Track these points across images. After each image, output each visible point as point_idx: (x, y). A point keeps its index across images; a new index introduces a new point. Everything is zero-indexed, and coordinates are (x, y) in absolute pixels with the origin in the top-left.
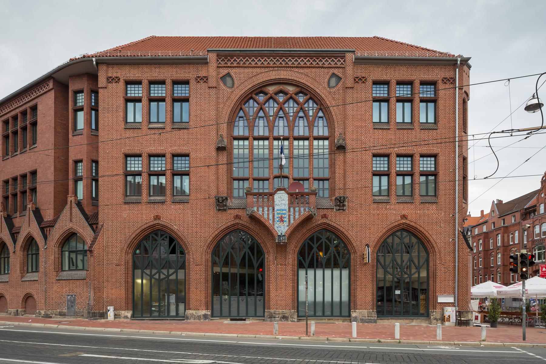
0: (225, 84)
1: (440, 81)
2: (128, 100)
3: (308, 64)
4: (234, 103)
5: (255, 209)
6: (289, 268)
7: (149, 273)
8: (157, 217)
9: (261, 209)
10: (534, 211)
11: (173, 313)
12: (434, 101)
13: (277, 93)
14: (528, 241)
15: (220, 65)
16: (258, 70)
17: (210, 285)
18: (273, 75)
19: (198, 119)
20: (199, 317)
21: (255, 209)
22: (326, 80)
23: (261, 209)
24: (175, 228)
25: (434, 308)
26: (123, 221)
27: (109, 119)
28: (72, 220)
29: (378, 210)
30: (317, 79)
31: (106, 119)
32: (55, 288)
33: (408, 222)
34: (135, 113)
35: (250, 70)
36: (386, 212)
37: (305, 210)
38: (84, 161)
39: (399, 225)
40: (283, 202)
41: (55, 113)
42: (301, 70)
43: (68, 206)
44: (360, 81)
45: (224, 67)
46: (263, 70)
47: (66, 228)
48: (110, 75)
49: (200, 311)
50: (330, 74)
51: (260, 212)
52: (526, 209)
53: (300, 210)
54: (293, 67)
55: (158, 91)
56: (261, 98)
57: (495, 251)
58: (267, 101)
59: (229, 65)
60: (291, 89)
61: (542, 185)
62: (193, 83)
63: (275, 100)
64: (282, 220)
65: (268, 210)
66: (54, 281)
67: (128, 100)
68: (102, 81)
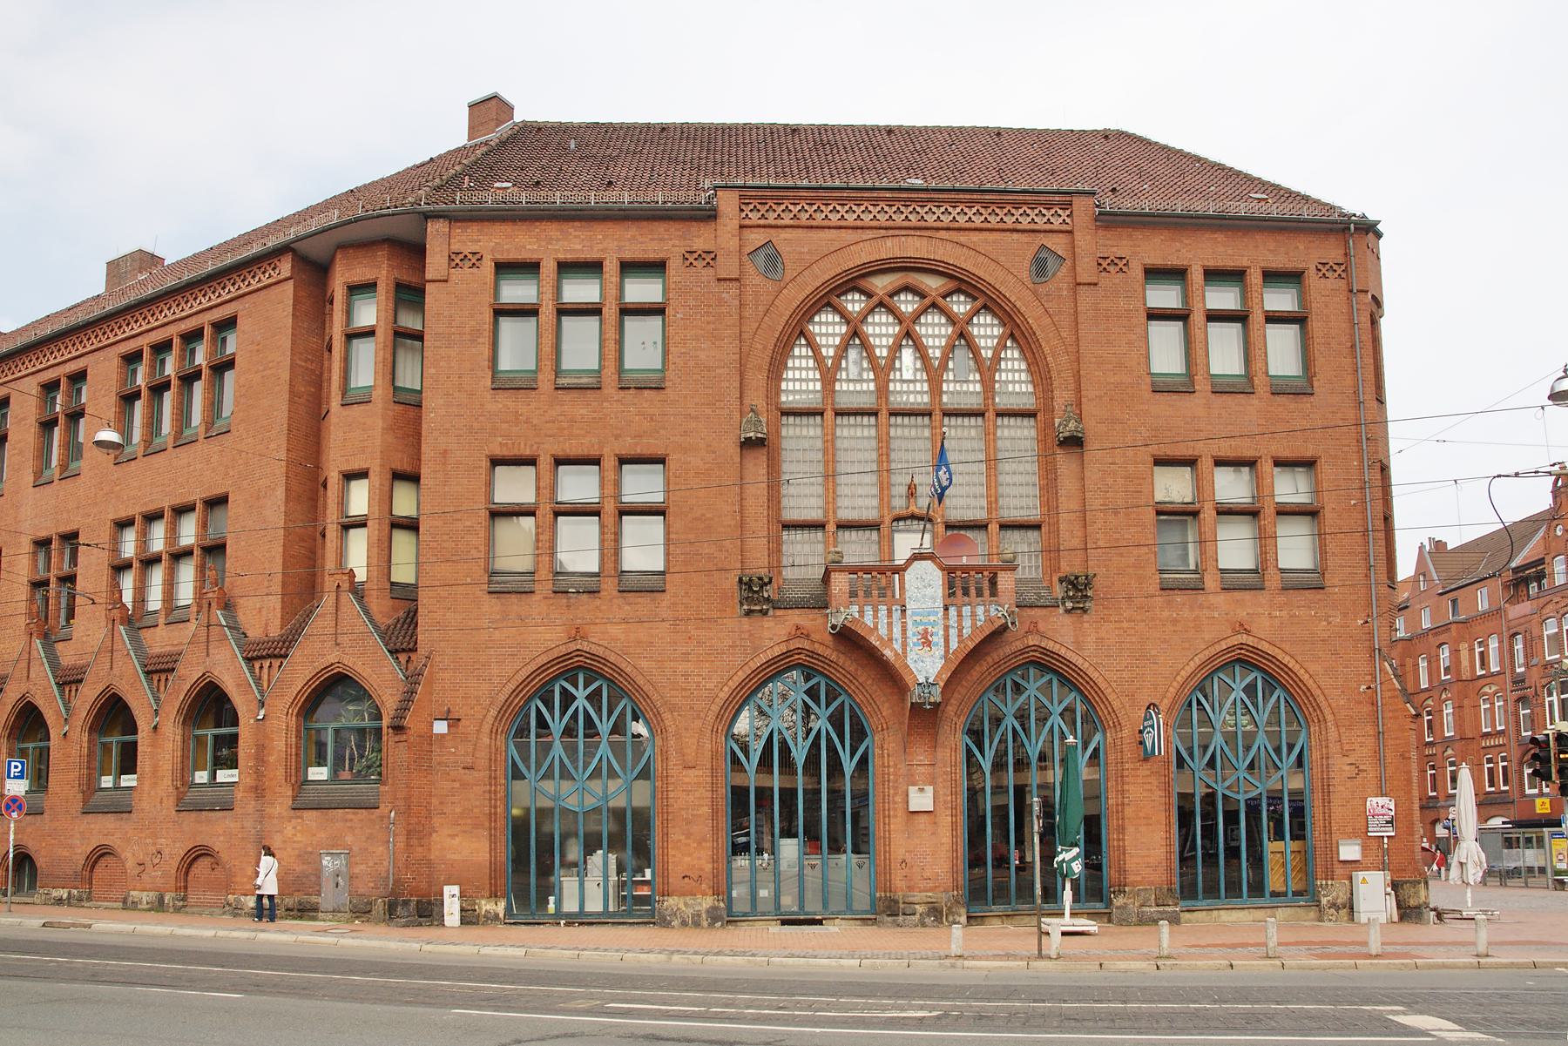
2: (501, 312)
3: (978, 220)
10: (1540, 577)
14: (1527, 665)
15: (747, 222)
18: (891, 248)
28: (342, 640)
32: (289, 831)
33: (1250, 641)
34: (517, 347)
38: (371, 473)
39: (1229, 650)
40: (929, 591)
41: (293, 343)
42: (962, 238)
44: (1112, 268)
45: (759, 226)
47: (320, 664)
48: (455, 248)
52: (1516, 570)
53: (973, 614)
54: (938, 229)
55: (580, 291)
56: (854, 304)
57: (1435, 693)
59: (771, 221)
60: (932, 284)
61: (1555, 498)
62: (674, 265)
63: (891, 311)
65: (890, 612)
67: (501, 312)
68: (436, 263)
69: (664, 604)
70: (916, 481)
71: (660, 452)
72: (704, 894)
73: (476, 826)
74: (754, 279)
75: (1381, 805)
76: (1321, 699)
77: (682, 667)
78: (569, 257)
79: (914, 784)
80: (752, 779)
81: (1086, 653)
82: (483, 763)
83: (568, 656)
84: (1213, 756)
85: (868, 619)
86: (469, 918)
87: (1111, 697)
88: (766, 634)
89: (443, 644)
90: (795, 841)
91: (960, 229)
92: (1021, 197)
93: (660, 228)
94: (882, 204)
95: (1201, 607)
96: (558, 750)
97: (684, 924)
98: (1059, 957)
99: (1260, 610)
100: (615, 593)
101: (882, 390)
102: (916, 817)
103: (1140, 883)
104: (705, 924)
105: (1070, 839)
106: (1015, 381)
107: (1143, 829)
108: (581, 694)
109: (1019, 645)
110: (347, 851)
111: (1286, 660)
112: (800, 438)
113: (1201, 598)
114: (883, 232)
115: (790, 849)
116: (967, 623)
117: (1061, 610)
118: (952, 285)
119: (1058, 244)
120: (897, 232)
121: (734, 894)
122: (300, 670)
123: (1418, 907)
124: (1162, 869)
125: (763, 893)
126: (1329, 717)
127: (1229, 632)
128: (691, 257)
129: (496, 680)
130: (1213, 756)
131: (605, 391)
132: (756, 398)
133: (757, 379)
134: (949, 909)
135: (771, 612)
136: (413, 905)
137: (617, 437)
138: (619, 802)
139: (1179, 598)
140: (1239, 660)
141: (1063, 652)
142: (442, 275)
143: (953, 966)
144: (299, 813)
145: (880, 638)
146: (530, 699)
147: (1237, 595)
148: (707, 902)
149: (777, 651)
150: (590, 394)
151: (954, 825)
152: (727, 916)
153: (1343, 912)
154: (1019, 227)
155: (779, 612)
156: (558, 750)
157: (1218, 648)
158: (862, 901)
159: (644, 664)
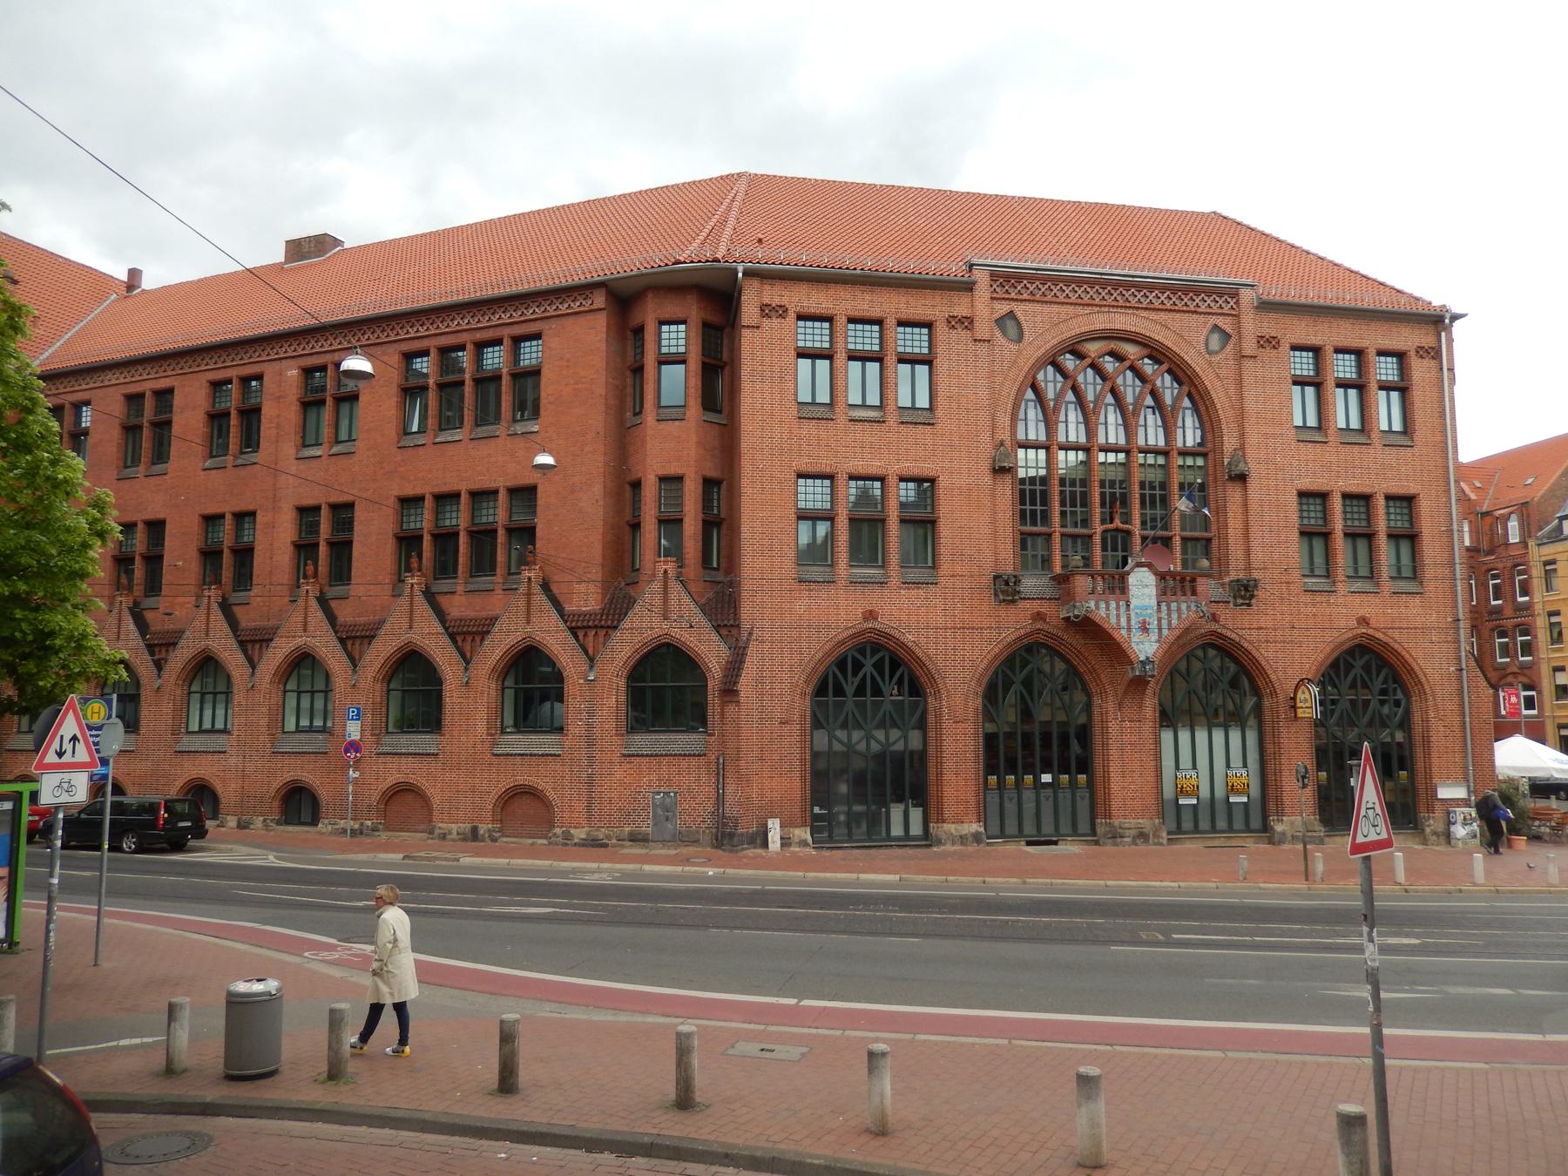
0: (1004, 333)
1: (1413, 353)
3: (1168, 305)
4: (1023, 373)
5: (1092, 604)
6: (1148, 727)
7: (835, 742)
8: (871, 615)
9: (1103, 605)
11: (897, 830)
12: (928, 361)
16: (1070, 309)
17: (932, 770)
19: (954, 405)
20: (963, 839)
21: (1092, 604)
22: (1202, 338)
23: (1103, 605)
24: (909, 638)
25: (1430, 809)
26: (794, 620)
29: (1314, 605)
30: (1185, 334)
31: (758, 395)
32: (619, 773)
33: (1370, 632)
35: (1055, 308)
36: (1328, 611)
37: (1188, 608)
40: (1146, 591)
42: (1153, 316)
46: (1080, 310)
47: (649, 635)
48: (766, 301)
49: (966, 826)
50: (1209, 325)
51: (1102, 612)
53: (1179, 609)
59: (1013, 295)
66: (616, 759)
68: (749, 310)
78: (857, 314)
118: (1146, 352)
122: (624, 647)
128: (954, 322)
133: (1004, 420)
153: (1442, 839)
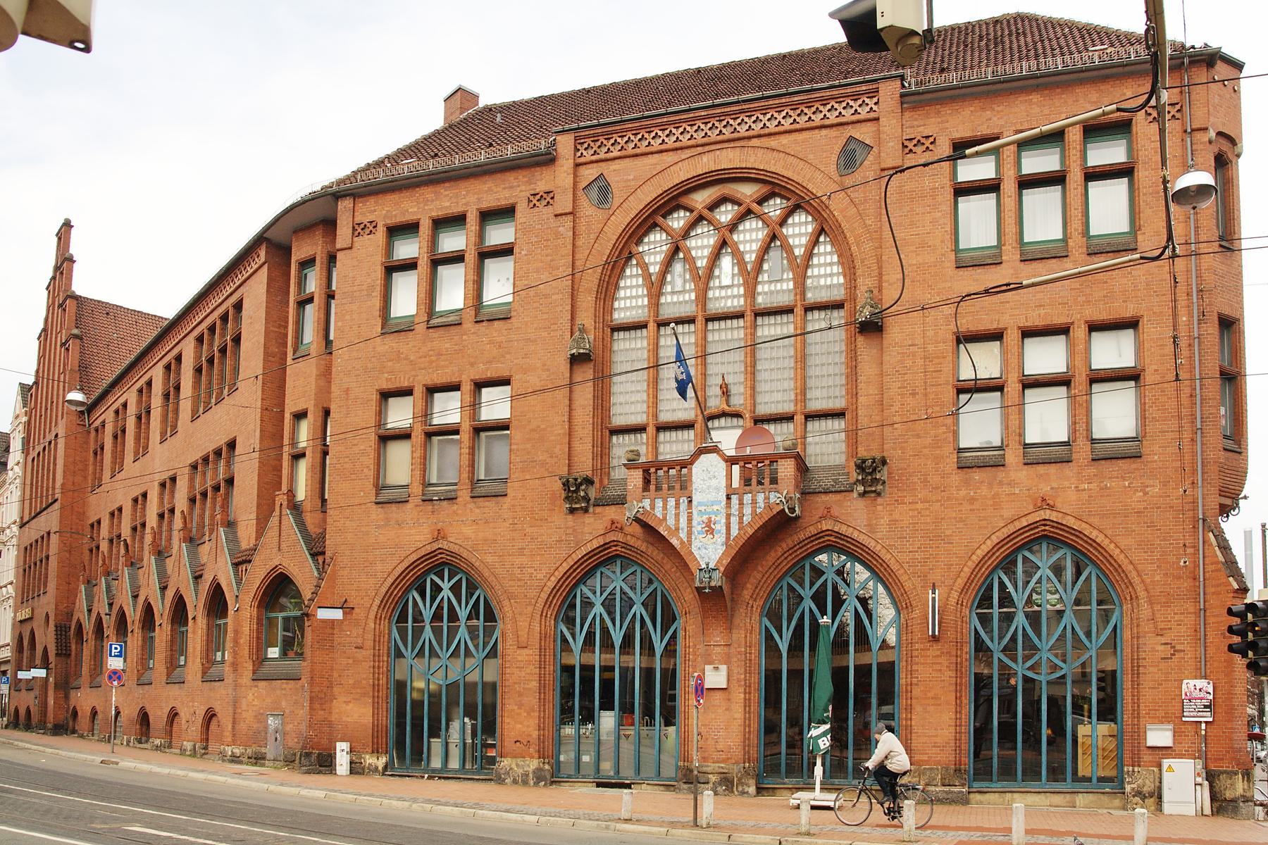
3: (787, 124)
9: (659, 503)
13: (713, 206)
23: (659, 503)
27: (355, 316)
32: (250, 697)
33: (1054, 516)
40: (714, 483)
41: (267, 313)
42: (772, 142)
43: (277, 513)
45: (592, 162)
48: (357, 220)
53: (754, 502)
54: (749, 138)
58: (790, 212)
60: (748, 191)
62: (521, 208)
64: (709, 529)
69: (505, 506)
70: (729, 380)
71: (506, 374)
72: (532, 757)
73: (364, 695)
74: (588, 209)
75: (1197, 687)
76: (1133, 575)
77: (519, 560)
79: (710, 664)
80: (576, 659)
81: (879, 535)
82: (370, 643)
83: (432, 554)
84: (1014, 639)
85: (658, 512)
86: (356, 769)
87: (903, 578)
88: (586, 529)
89: (343, 547)
90: (612, 713)
91: (770, 135)
92: (828, 93)
93: (511, 178)
94: (699, 123)
95: (1001, 483)
96: (428, 633)
97: (515, 782)
98: (709, 826)
99: (1066, 484)
100: (468, 498)
101: (702, 299)
102: (712, 693)
103: (927, 762)
104: (532, 783)
105: (818, 716)
106: (826, 275)
107: (931, 708)
108: (446, 585)
109: (813, 530)
110: (274, 709)
111: (1094, 534)
112: (630, 351)
113: (1000, 474)
114: (700, 149)
115: (608, 720)
116: (748, 510)
117: (855, 495)
118: (765, 189)
119: (864, 133)
120: (713, 147)
121: (562, 758)
123: (1234, 801)
124: (950, 749)
125: (586, 758)
126: (1142, 594)
127: (1031, 508)
129: (380, 575)
130: (1014, 639)
131: (464, 326)
132: (586, 318)
133: (587, 301)
134: (739, 779)
135: (591, 510)
136: (314, 757)
137: (472, 365)
138: (474, 677)
139: (977, 475)
140: (1045, 537)
141: (855, 535)
142: (347, 244)
143: (607, 828)
144: (256, 683)
145: (669, 528)
146: (407, 591)
147: (1041, 469)
148: (533, 764)
149: (595, 544)
150: (453, 330)
151: (747, 703)
152: (554, 776)
154: (827, 122)
155: (599, 509)
156: (428, 633)
157: (1018, 525)
158: (669, 771)
159: (489, 559)
